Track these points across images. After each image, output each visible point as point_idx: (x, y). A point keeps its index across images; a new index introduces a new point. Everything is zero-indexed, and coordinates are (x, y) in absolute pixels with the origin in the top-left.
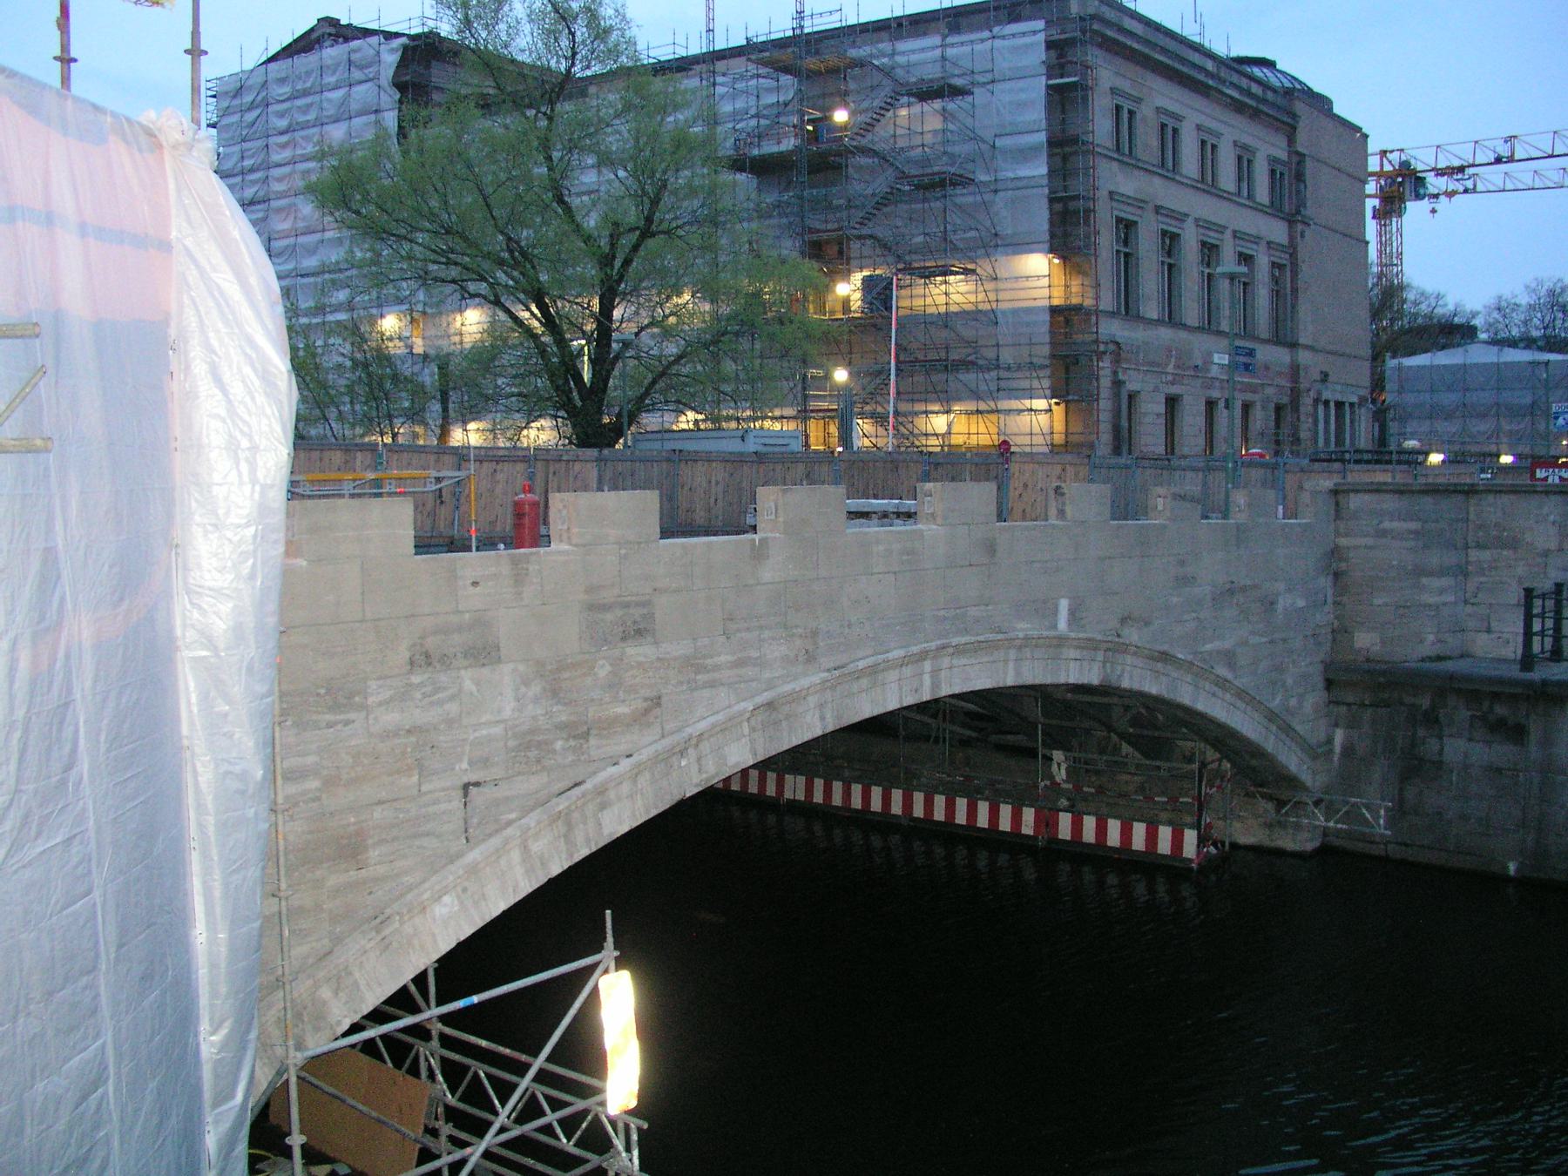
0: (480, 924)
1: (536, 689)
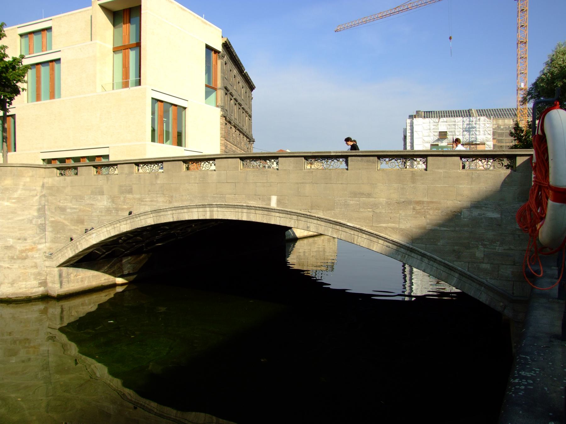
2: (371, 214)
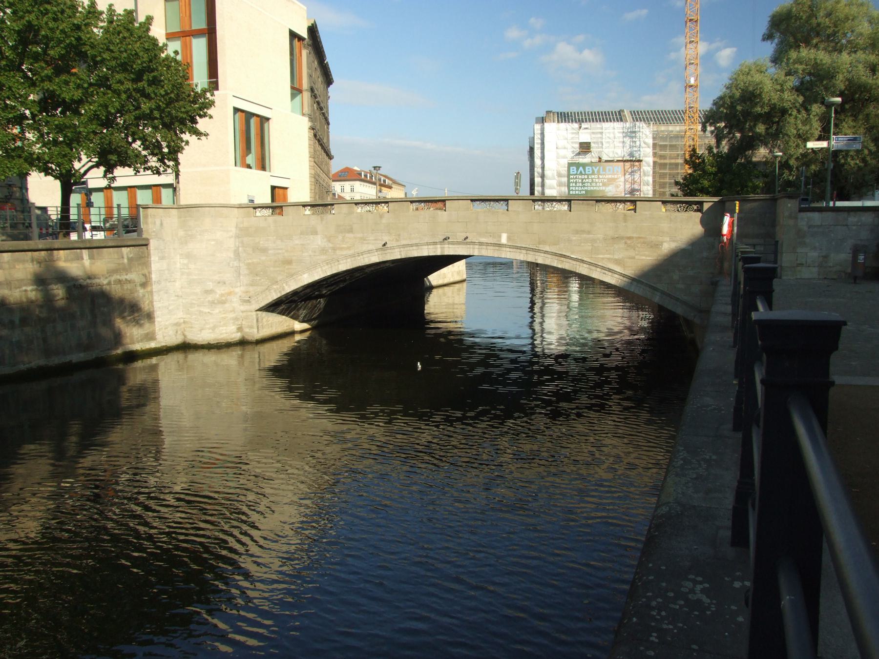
0: (403, 257)
1: (325, 240)
2: (590, 248)
